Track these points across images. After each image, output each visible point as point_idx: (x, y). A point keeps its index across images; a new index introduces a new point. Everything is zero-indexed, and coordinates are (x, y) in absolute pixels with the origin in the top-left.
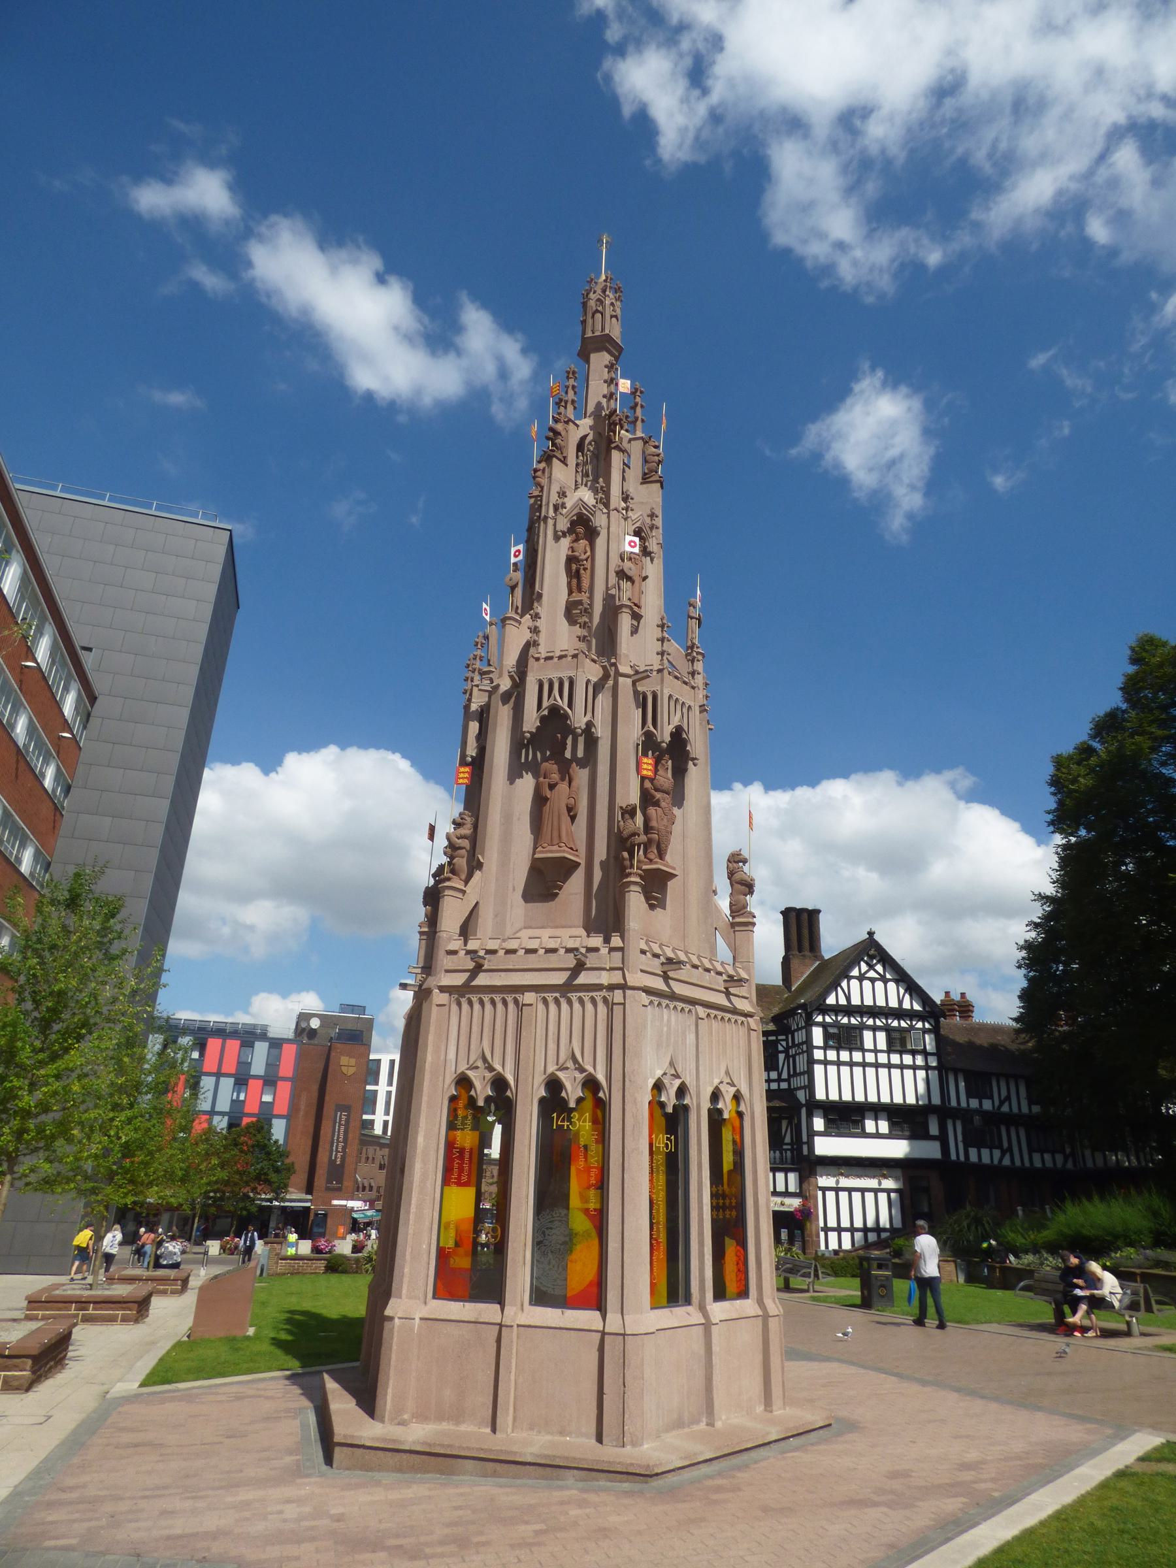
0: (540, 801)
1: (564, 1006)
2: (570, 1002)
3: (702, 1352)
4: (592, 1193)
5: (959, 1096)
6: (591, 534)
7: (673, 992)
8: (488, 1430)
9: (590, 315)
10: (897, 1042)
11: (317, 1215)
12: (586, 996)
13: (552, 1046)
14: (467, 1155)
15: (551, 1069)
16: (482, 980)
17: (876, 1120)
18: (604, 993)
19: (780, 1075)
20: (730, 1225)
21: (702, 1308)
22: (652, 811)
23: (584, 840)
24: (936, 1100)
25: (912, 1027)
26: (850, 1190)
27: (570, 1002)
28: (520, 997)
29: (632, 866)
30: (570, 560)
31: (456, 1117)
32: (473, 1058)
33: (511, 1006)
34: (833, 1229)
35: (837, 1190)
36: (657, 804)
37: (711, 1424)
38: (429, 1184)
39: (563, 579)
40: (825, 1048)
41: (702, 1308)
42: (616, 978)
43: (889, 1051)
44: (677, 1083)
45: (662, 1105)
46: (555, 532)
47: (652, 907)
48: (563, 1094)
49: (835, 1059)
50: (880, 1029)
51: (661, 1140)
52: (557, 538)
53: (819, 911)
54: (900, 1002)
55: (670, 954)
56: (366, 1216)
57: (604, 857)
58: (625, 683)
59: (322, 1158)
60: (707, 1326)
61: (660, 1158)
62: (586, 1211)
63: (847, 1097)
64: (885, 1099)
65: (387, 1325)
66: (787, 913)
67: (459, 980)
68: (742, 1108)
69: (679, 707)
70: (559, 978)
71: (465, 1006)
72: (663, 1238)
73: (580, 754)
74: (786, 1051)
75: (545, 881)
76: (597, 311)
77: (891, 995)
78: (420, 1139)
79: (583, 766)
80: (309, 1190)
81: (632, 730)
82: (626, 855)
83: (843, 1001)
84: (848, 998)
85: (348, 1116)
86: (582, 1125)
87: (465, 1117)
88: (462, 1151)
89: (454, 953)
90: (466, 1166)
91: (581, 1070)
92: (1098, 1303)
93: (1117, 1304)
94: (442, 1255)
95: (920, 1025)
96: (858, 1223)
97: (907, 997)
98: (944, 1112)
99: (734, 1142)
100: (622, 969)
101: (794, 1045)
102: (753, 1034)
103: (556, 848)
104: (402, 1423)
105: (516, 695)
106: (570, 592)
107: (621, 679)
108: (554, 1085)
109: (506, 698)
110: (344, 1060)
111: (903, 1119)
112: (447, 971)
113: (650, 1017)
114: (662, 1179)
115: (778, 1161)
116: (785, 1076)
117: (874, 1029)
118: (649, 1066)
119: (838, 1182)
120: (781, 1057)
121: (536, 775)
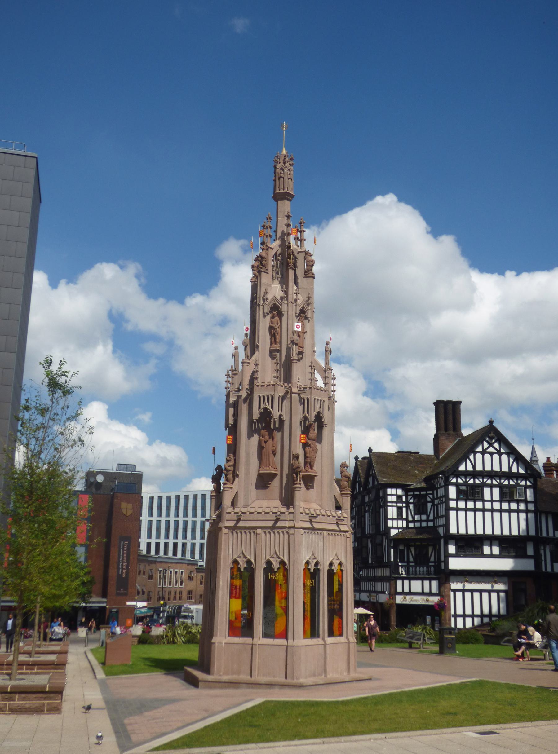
0: (261, 448)
1: (272, 534)
2: (274, 533)
3: (323, 653)
4: (283, 601)
5: (549, 530)
6: (280, 315)
7: (314, 527)
8: (249, 677)
9: (277, 178)
10: (507, 495)
11: (111, 612)
12: (280, 531)
13: (268, 549)
14: (238, 588)
15: (268, 557)
16: (241, 524)
17: (491, 546)
18: (287, 530)
19: (428, 517)
20: (336, 611)
21: (323, 639)
22: (307, 449)
23: (278, 465)
24: (532, 533)
25: (518, 484)
26: (472, 591)
27: (274, 533)
28: (255, 531)
29: (297, 480)
30: (271, 328)
31: (233, 574)
32: (239, 553)
33: (252, 534)
34: (469, 616)
35: (463, 591)
36: (309, 446)
37: (326, 676)
38: (225, 598)
39: (268, 336)
40: (457, 500)
41: (323, 639)
42: (291, 524)
43: (501, 501)
44: (315, 561)
45: (309, 569)
46: (264, 313)
47: (308, 489)
48: (272, 566)
49: (464, 507)
50: (495, 486)
51: (309, 582)
52: (265, 316)
53: (460, 402)
54: (510, 468)
55: (313, 512)
56: (141, 613)
57: (287, 472)
58: (295, 397)
59: (112, 573)
60: (325, 645)
61: (308, 588)
62: (281, 607)
63: (471, 531)
64: (497, 532)
65: (213, 646)
66: (438, 404)
67: (232, 524)
68: (342, 568)
69: (319, 403)
70: (270, 524)
71: (235, 534)
72: (309, 615)
73: (277, 425)
74: (432, 501)
75: (264, 481)
76: (281, 177)
77: (503, 463)
78: (221, 583)
79: (278, 431)
80: (104, 594)
81: (298, 417)
82: (295, 475)
83: (470, 468)
84: (474, 466)
85: (129, 544)
86: (280, 577)
87: (237, 575)
88: (236, 587)
89: (230, 513)
90: (238, 592)
91: (279, 558)
92: (531, 646)
93: (538, 646)
94: (231, 623)
95: (523, 483)
96: (477, 612)
97: (515, 464)
98: (538, 540)
99: (339, 581)
100: (293, 520)
101: (437, 498)
102: (348, 539)
103: (268, 468)
104: (220, 675)
105: (249, 399)
106: (271, 344)
107: (293, 395)
108: (269, 563)
109: (245, 400)
110: (124, 505)
111: (509, 545)
112: (227, 520)
113: (304, 539)
114: (309, 596)
115: (425, 573)
116: (431, 517)
117: (491, 486)
118: (304, 556)
119: (464, 586)
120: (429, 505)
121: (259, 435)
